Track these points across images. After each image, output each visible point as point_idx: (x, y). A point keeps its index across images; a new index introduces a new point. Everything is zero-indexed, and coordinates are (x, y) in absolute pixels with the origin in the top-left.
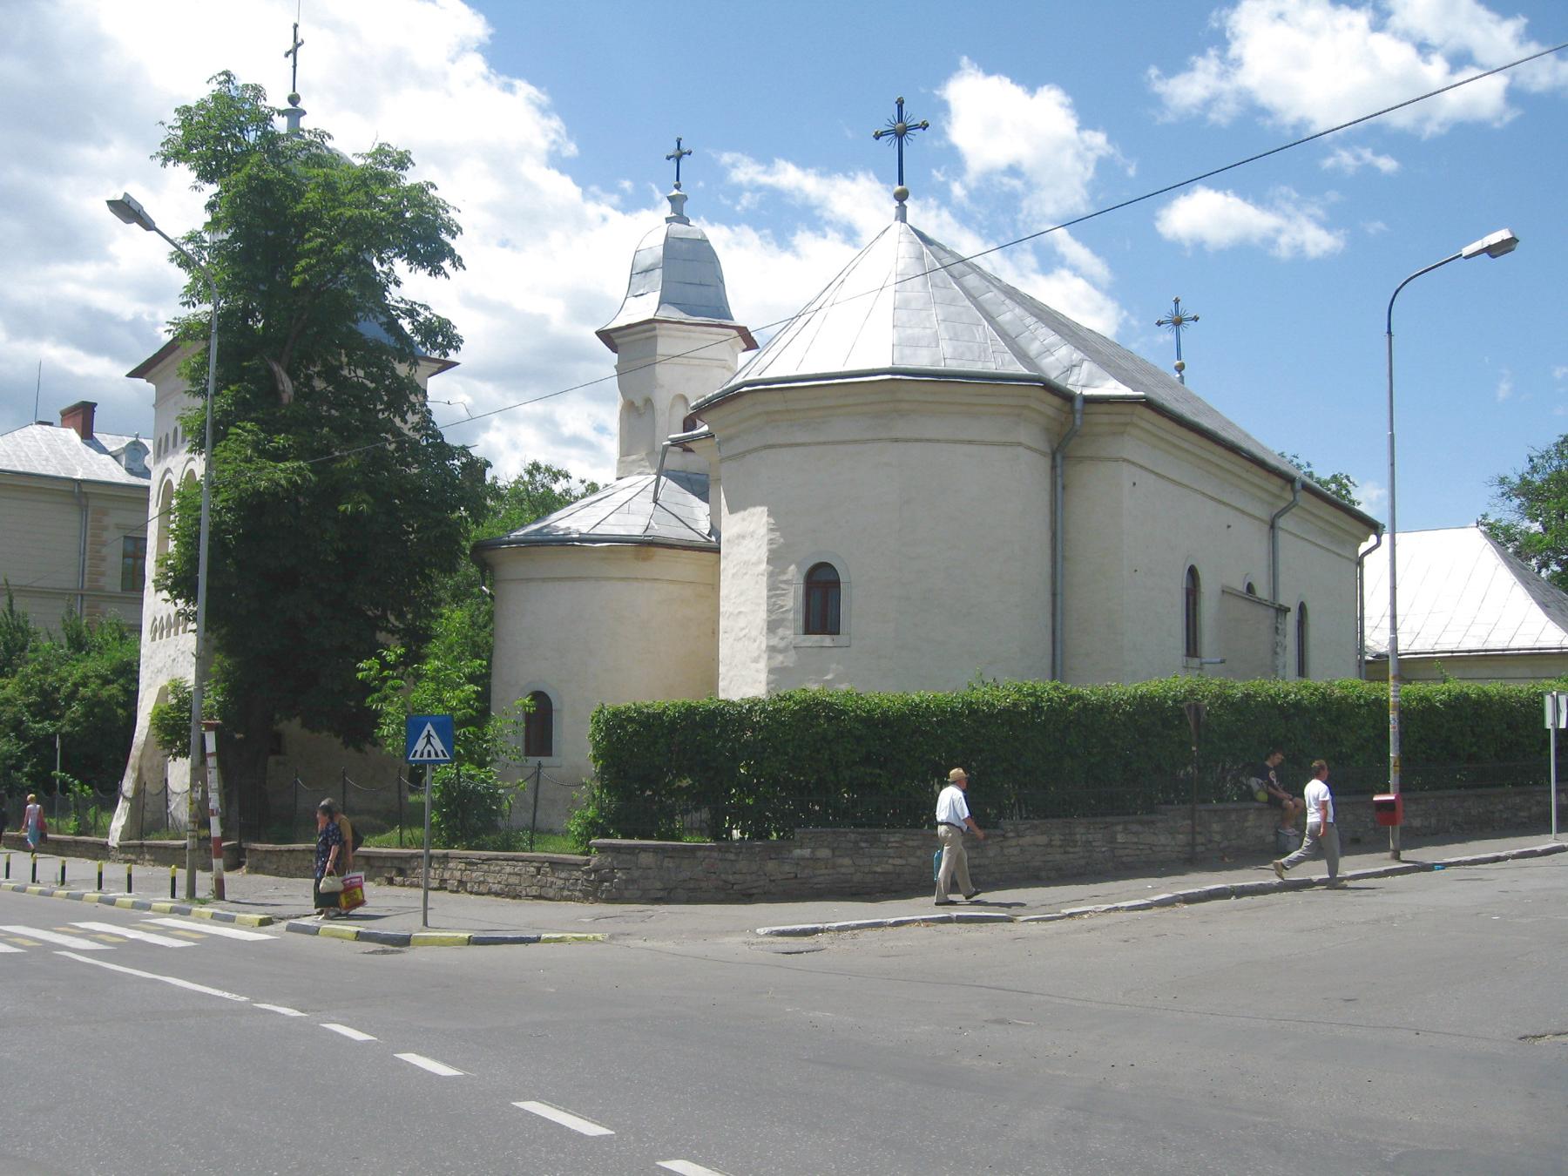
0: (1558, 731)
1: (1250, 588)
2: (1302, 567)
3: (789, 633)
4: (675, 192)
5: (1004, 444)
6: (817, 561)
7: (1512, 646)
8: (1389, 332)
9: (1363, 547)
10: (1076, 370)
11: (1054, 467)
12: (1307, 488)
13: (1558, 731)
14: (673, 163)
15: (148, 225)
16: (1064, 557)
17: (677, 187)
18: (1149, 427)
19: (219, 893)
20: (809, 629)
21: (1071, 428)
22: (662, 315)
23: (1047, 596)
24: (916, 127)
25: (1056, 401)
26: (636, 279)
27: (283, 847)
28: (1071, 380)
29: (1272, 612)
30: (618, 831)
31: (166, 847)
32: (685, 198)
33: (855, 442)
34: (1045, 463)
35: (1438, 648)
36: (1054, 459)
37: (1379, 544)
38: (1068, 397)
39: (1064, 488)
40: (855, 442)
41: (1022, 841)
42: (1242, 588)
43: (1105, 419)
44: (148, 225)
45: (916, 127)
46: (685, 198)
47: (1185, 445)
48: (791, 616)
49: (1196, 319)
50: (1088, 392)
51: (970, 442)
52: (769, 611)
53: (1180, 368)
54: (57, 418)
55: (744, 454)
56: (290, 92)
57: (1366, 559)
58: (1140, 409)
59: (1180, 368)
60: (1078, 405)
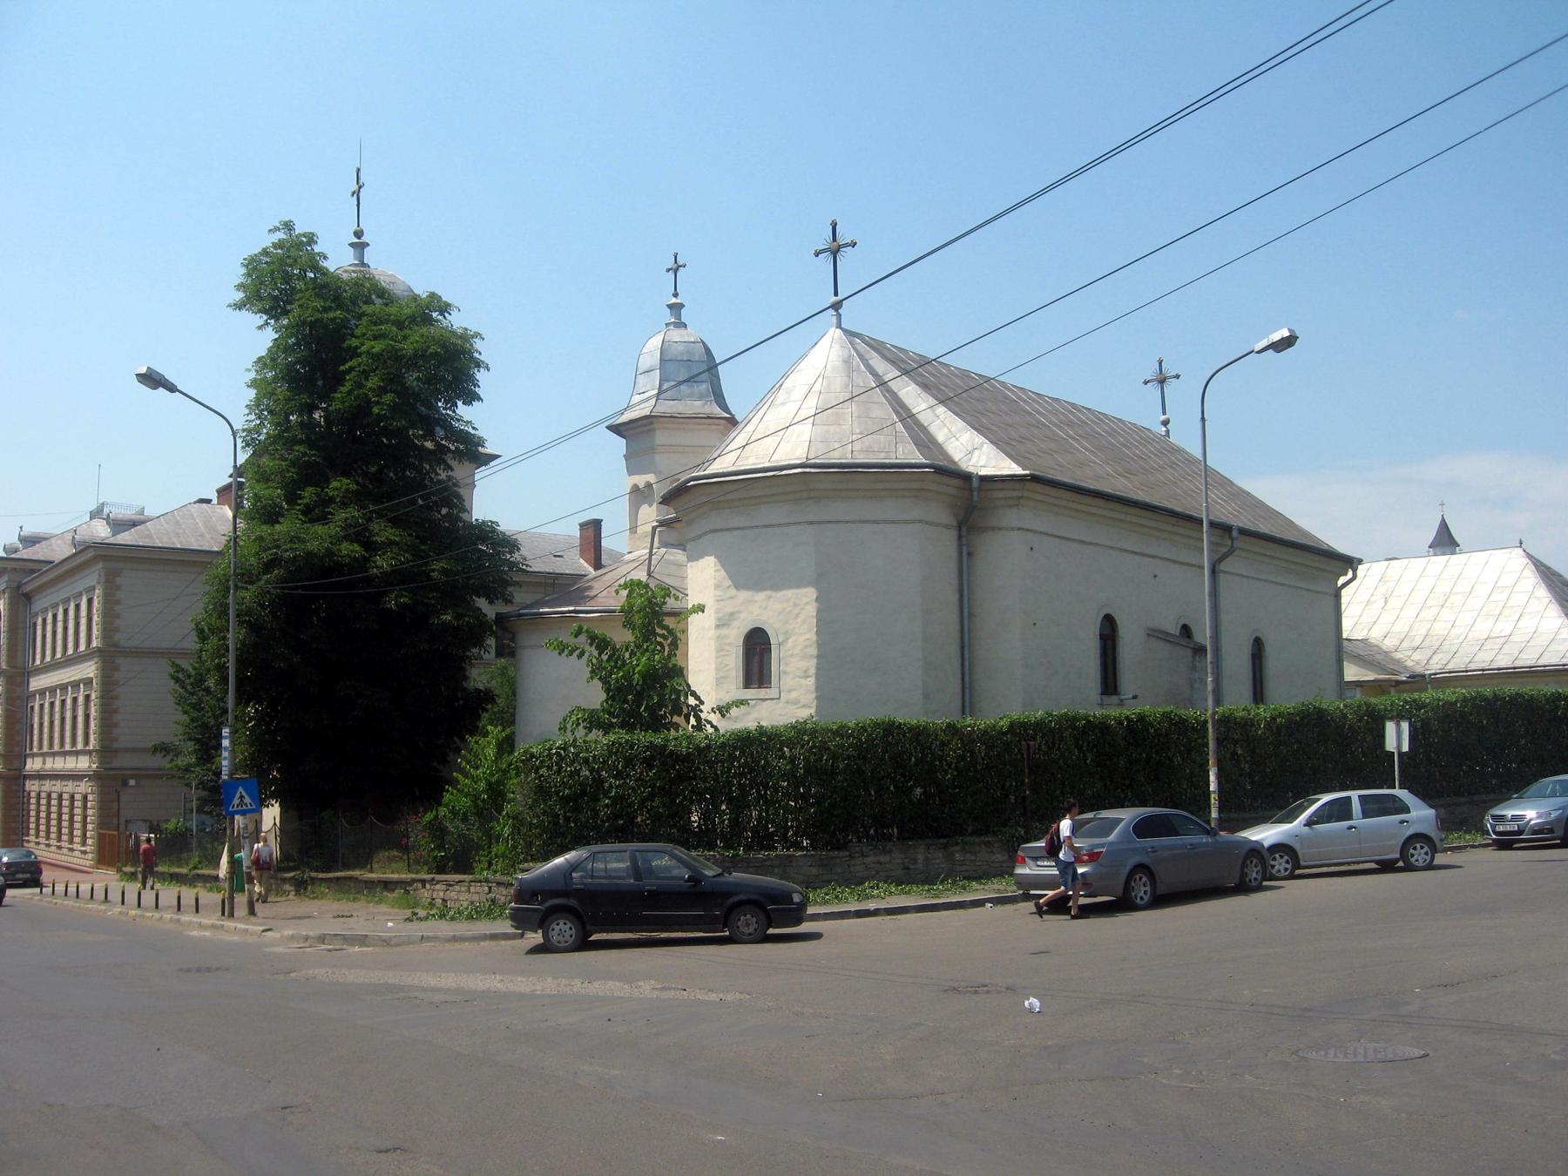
0: (1401, 754)
1: (1186, 631)
2: (1254, 602)
3: (733, 687)
4: (674, 300)
5: (906, 522)
6: (746, 630)
7: (1541, 662)
8: (1203, 419)
9: (1342, 580)
10: (977, 453)
11: (960, 538)
12: (1244, 532)
13: (1401, 754)
14: (671, 274)
15: (172, 388)
16: (970, 614)
17: (676, 295)
18: (1040, 497)
19: (252, 912)
20: (748, 684)
21: (969, 503)
22: (667, 407)
23: (955, 648)
24: (846, 245)
25: (957, 482)
26: (641, 379)
27: (331, 875)
28: (973, 461)
29: (1189, 653)
30: (535, 859)
31: (338, 879)
32: (682, 306)
33: (779, 525)
34: (954, 533)
35: (1472, 666)
36: (960, 529)
37: (1354, 578)
38: (967, 477)
39: (969, 554)
40: (779, 525)
41: (867, 860)
42: (1174, 629)
43: (1001, 494)
44: (172, 388)
45: (846, 245)
46: (682, 306)
47: (1093, 510)
48: (734, 673)
49: (1177, 377)
50: (983, 472)
51: (876, 522)
52: (718, 669)
53: (1165, 423)
54: (214, 497)
55: (700, 537)
56: (355, 227)
57: (1344, 592)
58: (1029, 485)
59: (1165, 423)
60: (975, 483)
